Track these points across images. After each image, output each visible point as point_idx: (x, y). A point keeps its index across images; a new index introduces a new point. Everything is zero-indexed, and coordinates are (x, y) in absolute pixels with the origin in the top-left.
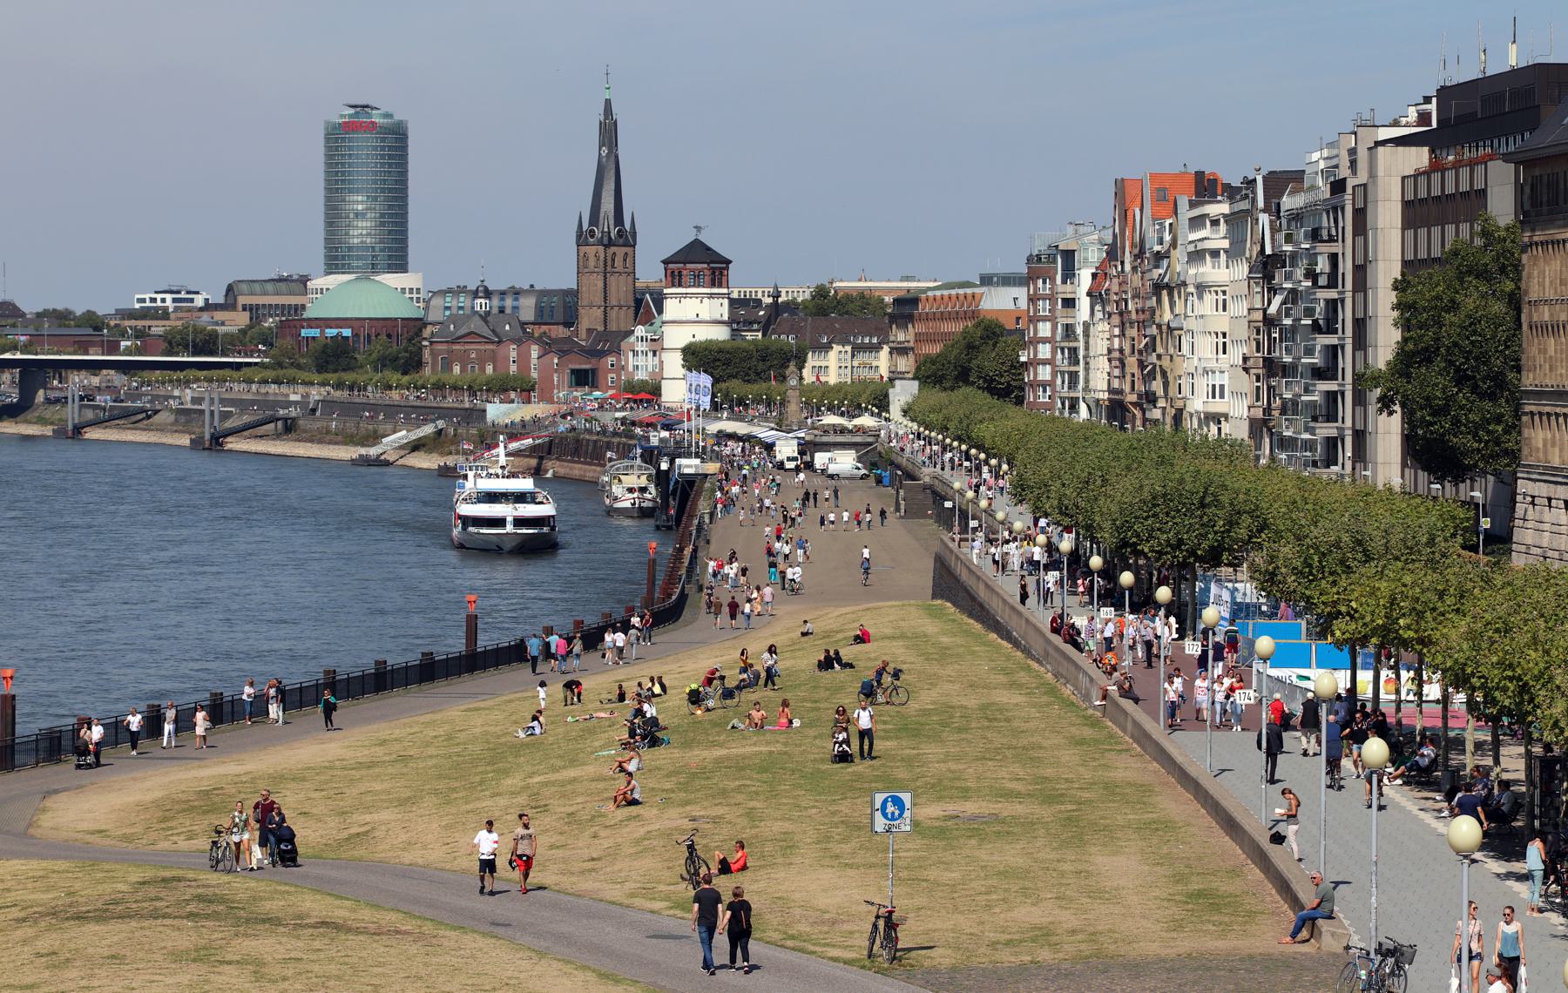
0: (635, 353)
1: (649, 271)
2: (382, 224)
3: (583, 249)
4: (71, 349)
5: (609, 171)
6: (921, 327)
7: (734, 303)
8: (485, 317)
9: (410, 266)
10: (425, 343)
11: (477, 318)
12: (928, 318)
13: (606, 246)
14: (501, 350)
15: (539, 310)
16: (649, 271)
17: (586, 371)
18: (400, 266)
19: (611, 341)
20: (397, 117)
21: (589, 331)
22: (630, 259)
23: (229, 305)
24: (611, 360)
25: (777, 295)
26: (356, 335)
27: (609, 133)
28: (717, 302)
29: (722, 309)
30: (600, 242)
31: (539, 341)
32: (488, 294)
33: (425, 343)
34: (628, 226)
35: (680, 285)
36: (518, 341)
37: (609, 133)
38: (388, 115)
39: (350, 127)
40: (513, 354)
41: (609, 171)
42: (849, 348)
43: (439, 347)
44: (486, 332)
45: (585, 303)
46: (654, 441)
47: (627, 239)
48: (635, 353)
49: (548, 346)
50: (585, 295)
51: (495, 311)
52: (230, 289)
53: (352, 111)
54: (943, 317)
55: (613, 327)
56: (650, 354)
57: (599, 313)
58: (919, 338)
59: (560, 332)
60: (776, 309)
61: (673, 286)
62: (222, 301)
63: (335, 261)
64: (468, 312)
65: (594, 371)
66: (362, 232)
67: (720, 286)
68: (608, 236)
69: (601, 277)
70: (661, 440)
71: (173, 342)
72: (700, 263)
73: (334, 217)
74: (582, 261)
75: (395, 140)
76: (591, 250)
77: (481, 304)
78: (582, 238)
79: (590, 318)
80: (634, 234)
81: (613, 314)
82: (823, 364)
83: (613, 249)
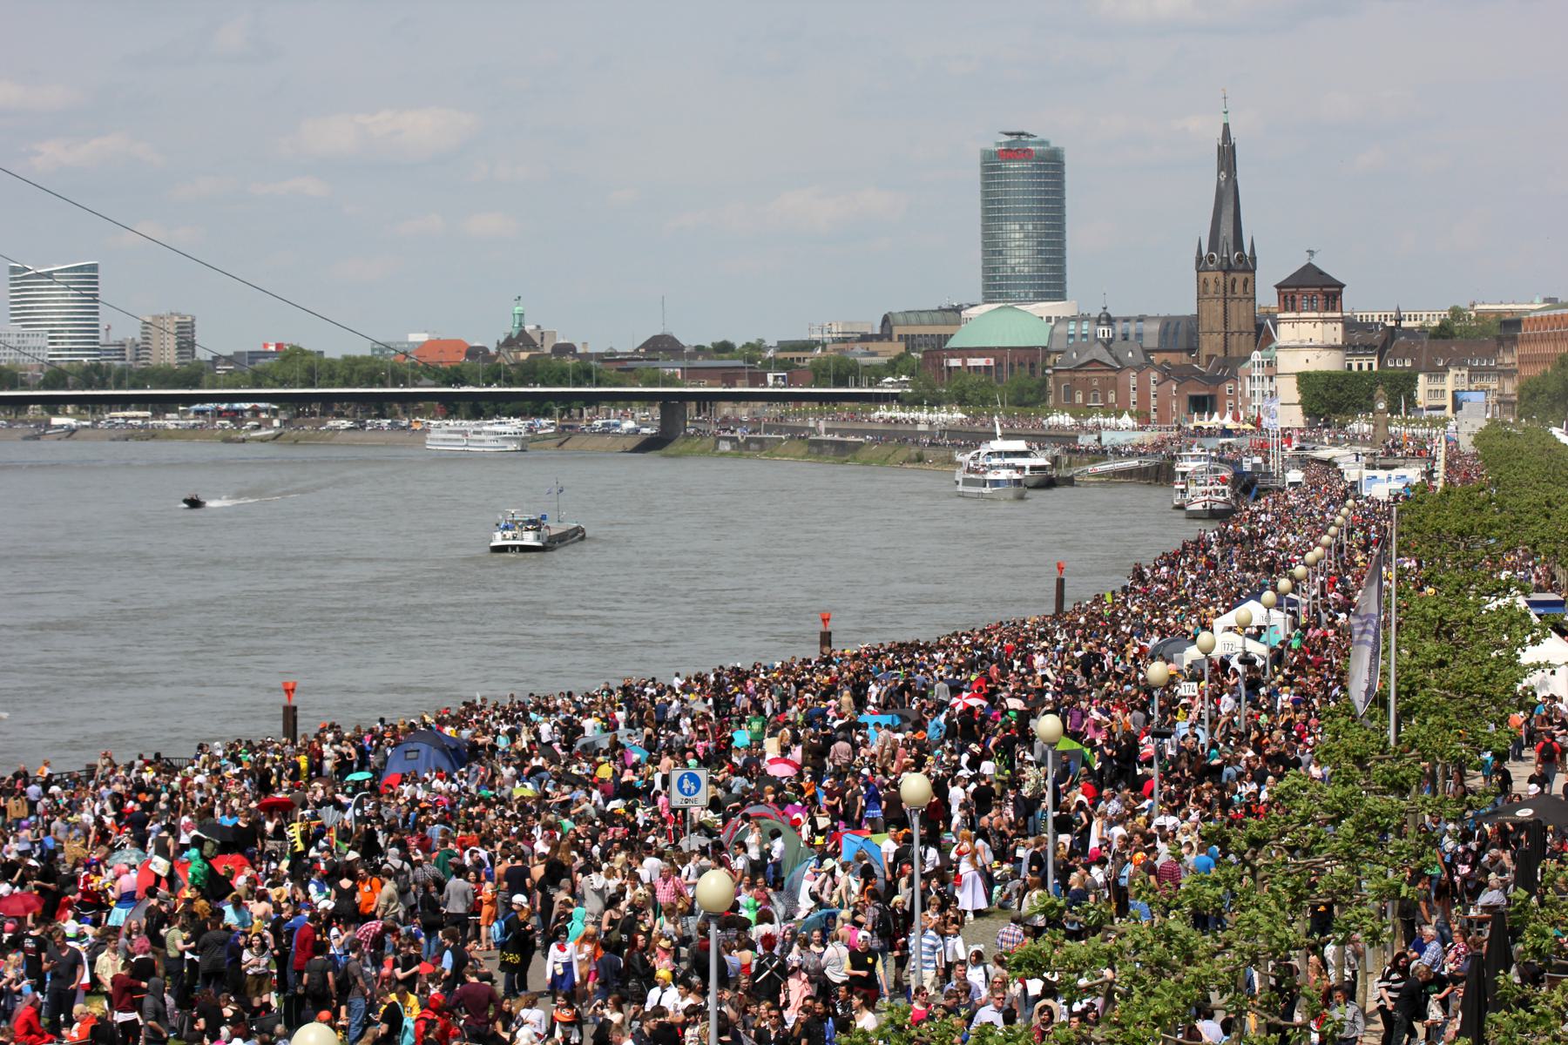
0: (1252, 379)
1: (1267, 297)
2: (1040, 252)
3: (1203, 275)
4: (425, 381)
5: (1228, 198)
6: (1525, 349)
7: (1350, 325)
8: (1107, 344)
9: (1068, 294)
10: (1049, 371)
11: (1099, 345)
12: (1529, 340)
13: (1225, 272)
14: (1121, 377)
15: (1164, 333)
16: (1267, 297)
17: (1204, 397)
18: (1058, 294)
19: (1230, 366)
20: (1053, 145)
21: (1210, 357)
22: (1249, 285)
23: (885, 334)
24: (1228, 386)
25: (1399, 320)
26: (998, 364)
27: (1227, 156)
28: (1330, 326)
29: (1335, 333)
30: (1220, 268)
31: (1159, 368)
32: (1110, 321)
33: (1049, 371)
34: (1247, 251)
35: (1293, 310)
36: (1139, 369)
37: (1227, 156)
38: (1043, 143)
39: (1009, 153)
40: (1133, 381)
41: (1228, 198)
42: (1466, 372)
43: (1061, 375)
44: (1108, 360)
45: (1206, 329)
46: (1247, 467)
47: (1247, 265)
48: (1252, 379)
49: (1167, 373)
50: (1205, 322)
51: (1119, 338)
52: (886, 320)
53: (1008, 139)
54: (1543, 339)
55: (1234, 352)
56: (1267, 380)
57: (1219, 339)
58: (1524, 361)
59: (1183, 358)
60: (1392, 333)
61: (1286, 310)
62: (878, 331)
63: (996, 287)
64: (1092, 339)
65: (1212, 397)
66: (1020, 255)
67: (1334, 310)
68: (1227, 260)
69: (1221, 303)
70: (1254, 466)
71: (819, 373)
72: (1313, 288)
73: (992, 248)
74: (1202, 286)
75: (1051, 166)
76: (1210, 276)
77: (1103, 331)
78: (1201, 264)
79: (1211, 344)
80: (1254, 259)
81: (1233, 340)
82: (1440, 387)
83: (1233, 275)
